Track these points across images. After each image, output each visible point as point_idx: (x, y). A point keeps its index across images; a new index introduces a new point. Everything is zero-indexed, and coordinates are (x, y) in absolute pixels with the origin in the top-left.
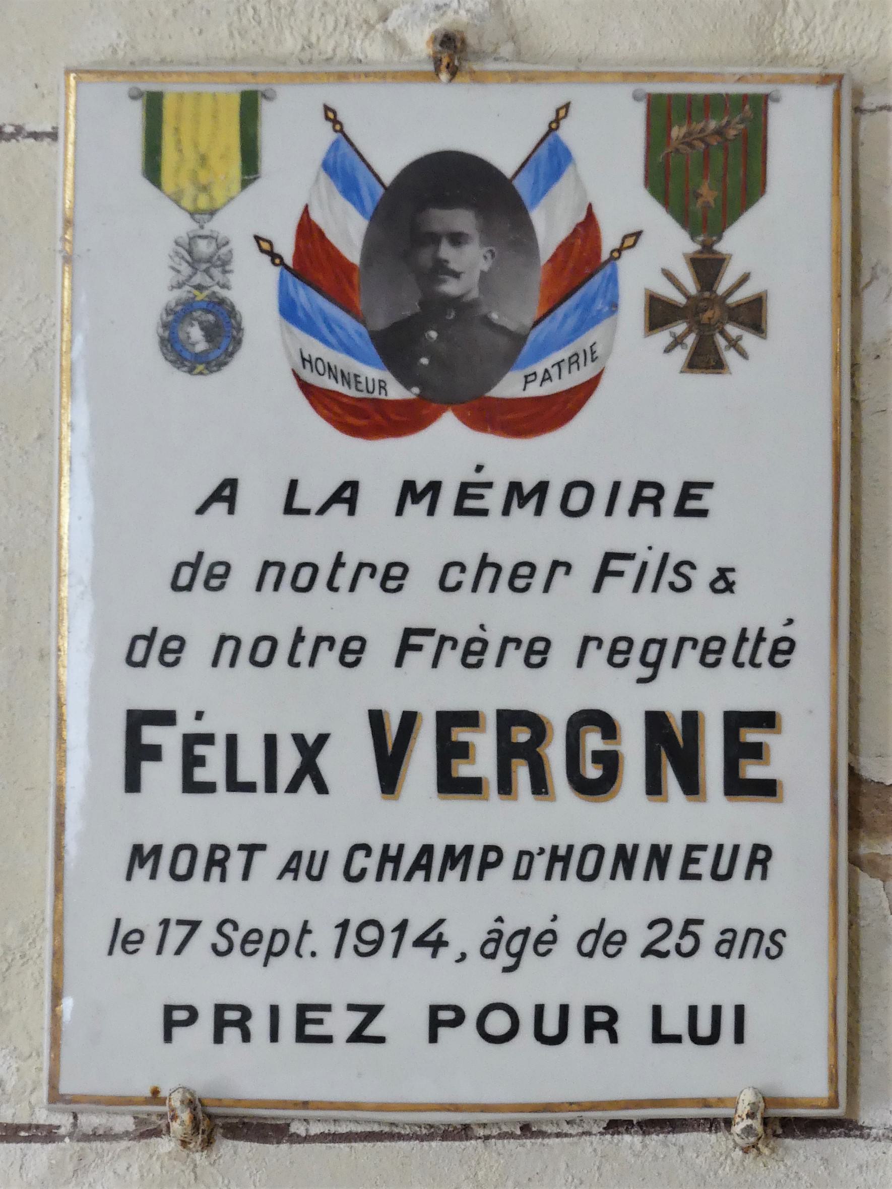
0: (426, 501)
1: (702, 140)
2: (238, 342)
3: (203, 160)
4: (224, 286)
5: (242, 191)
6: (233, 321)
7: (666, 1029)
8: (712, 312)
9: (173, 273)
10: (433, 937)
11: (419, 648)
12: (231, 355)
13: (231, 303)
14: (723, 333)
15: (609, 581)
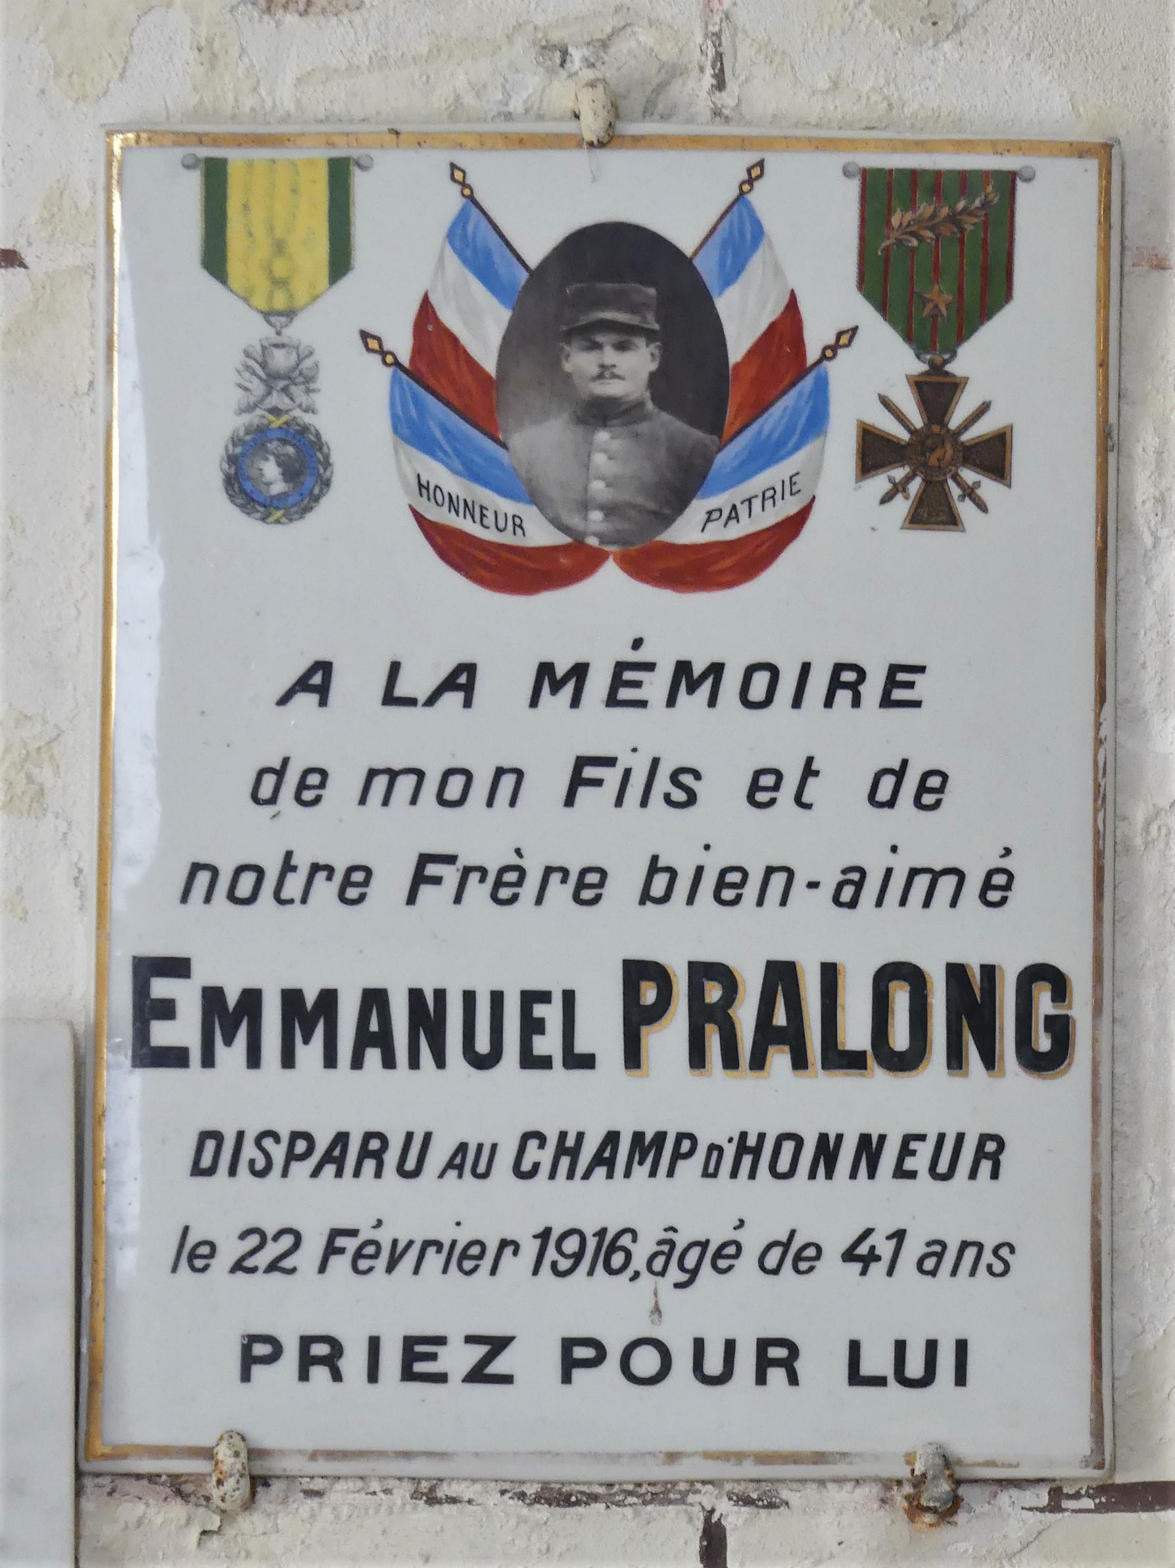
0: (568, 690)
1: (931, 229)
2: (327, 484)
3: (279, 248)
4: (310, 410)
6: (319, 455)
7: (866, 1369)
9: (241, 392)
10: (863, 1250)
11: (437, 880)
12: (317, 499)
14: (956, 478)
15: (583, 792)
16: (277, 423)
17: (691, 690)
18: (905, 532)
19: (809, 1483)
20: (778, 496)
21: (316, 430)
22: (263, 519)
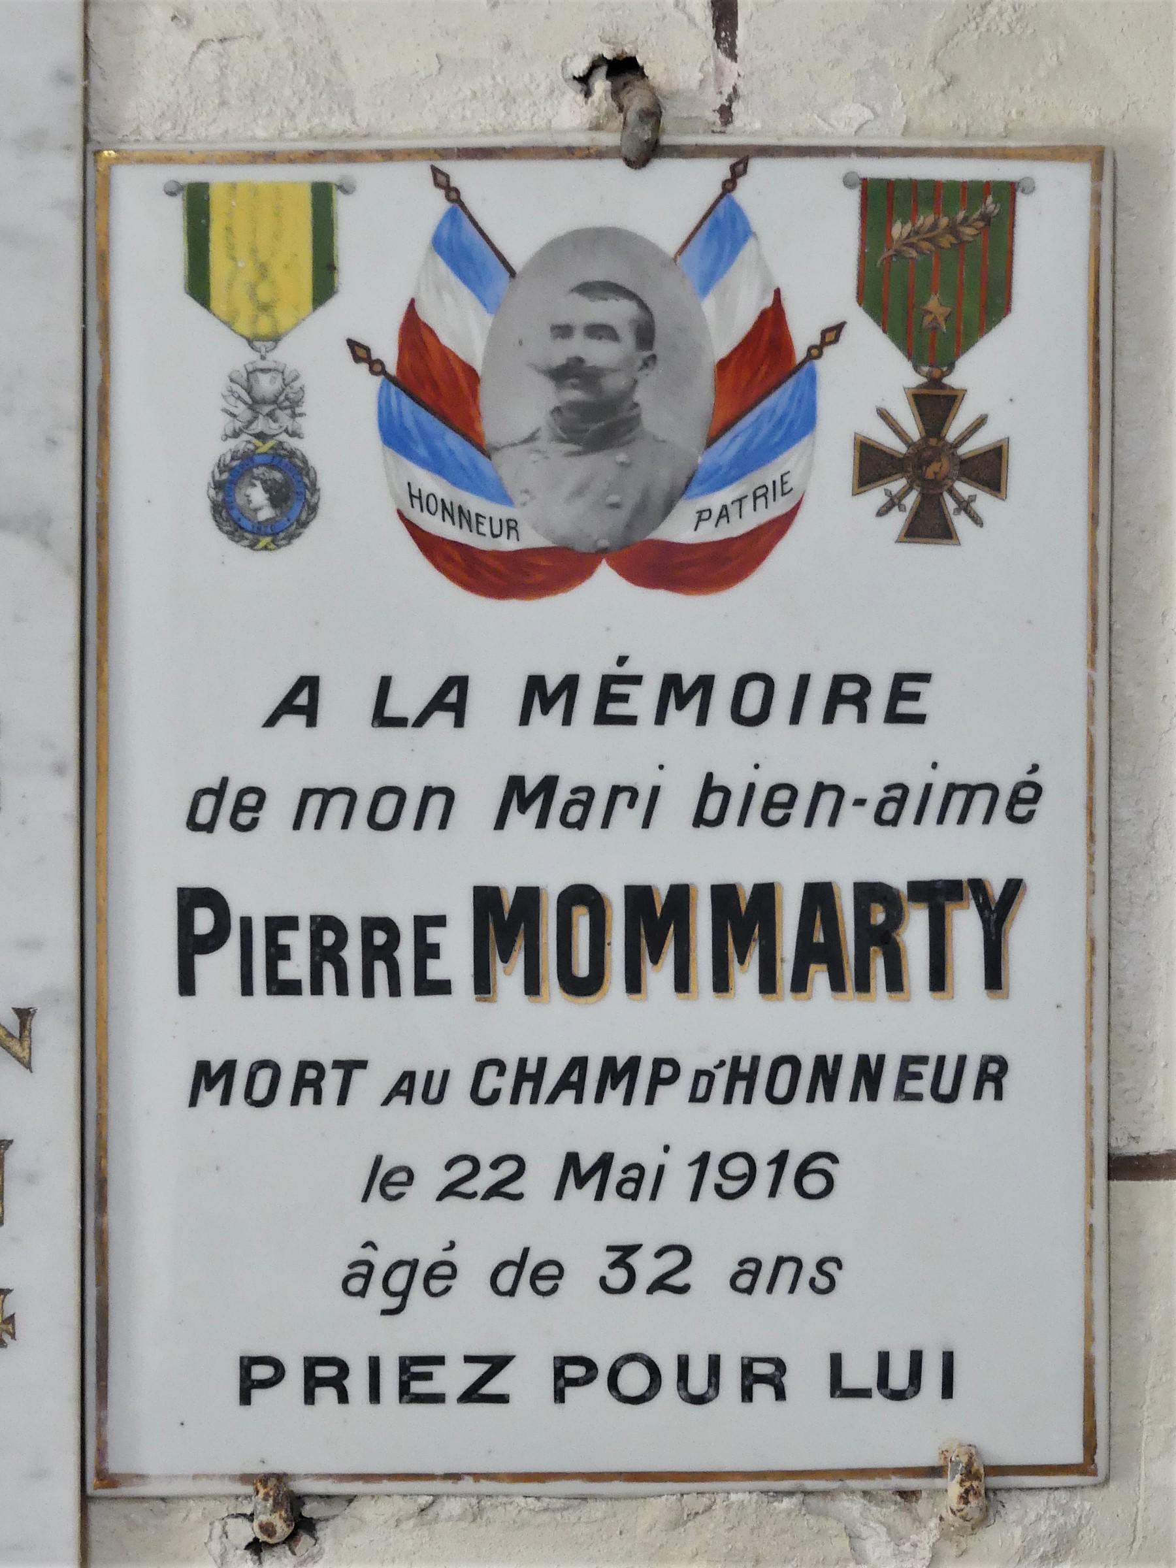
2: (313, 509)
3: (263, 271)
5: (315, 309)
7: (848, 1382)
8: (939, 464)
9: (228, 418)
12: (304, 524)
13: (303, 456)
14: (951, 491)
16: (265, 448)
17: (680, 706)
18: (899, 545)
19: (1003, 1491)
20: (770, 495)
21: (302, 454)
22: (252, 546)
